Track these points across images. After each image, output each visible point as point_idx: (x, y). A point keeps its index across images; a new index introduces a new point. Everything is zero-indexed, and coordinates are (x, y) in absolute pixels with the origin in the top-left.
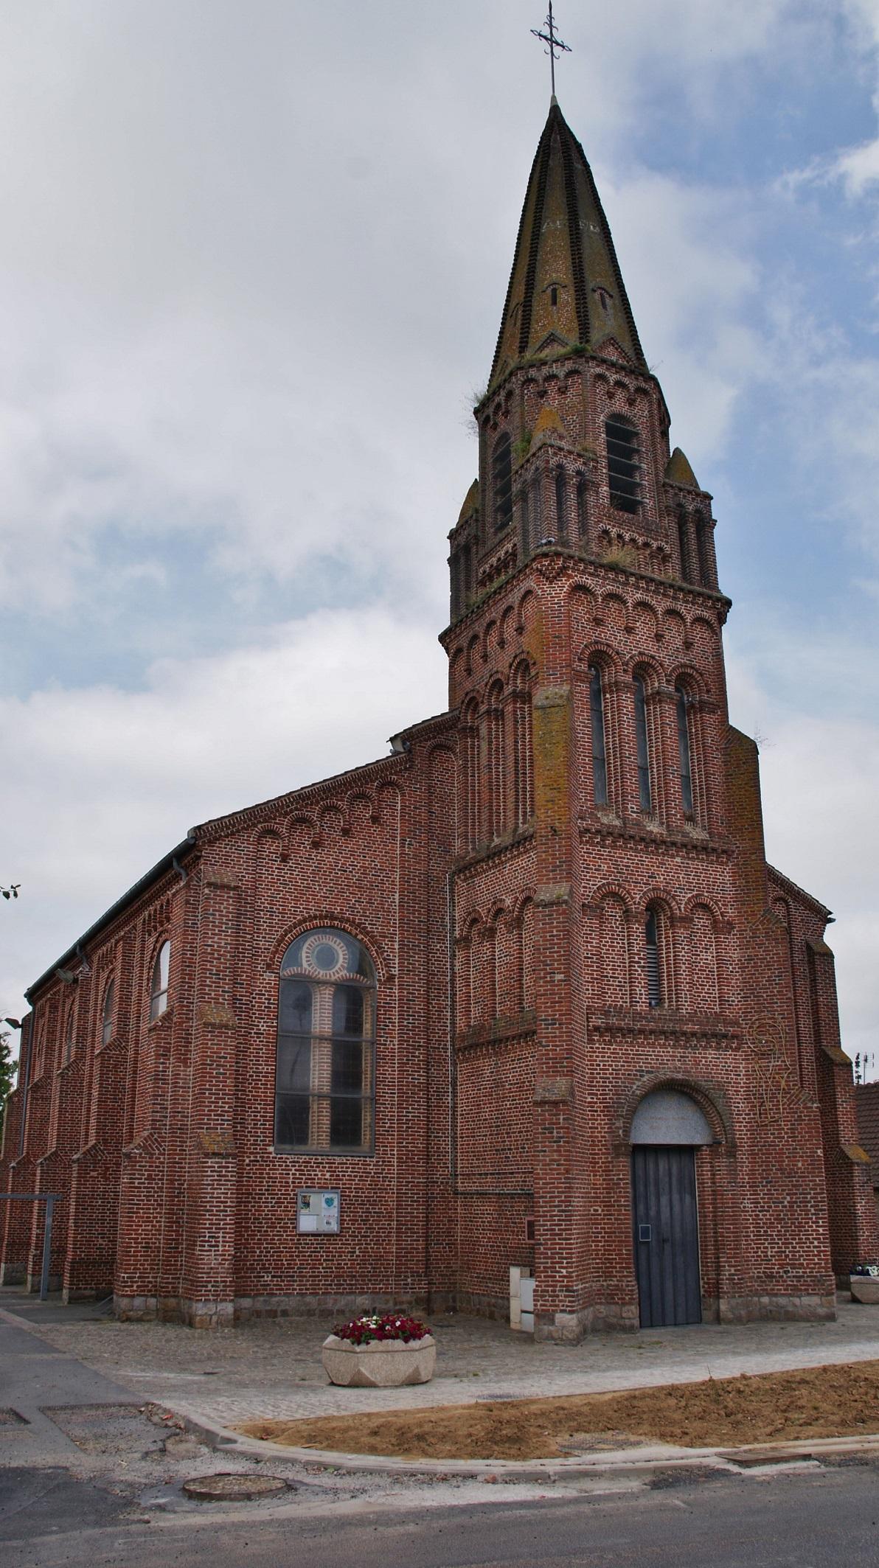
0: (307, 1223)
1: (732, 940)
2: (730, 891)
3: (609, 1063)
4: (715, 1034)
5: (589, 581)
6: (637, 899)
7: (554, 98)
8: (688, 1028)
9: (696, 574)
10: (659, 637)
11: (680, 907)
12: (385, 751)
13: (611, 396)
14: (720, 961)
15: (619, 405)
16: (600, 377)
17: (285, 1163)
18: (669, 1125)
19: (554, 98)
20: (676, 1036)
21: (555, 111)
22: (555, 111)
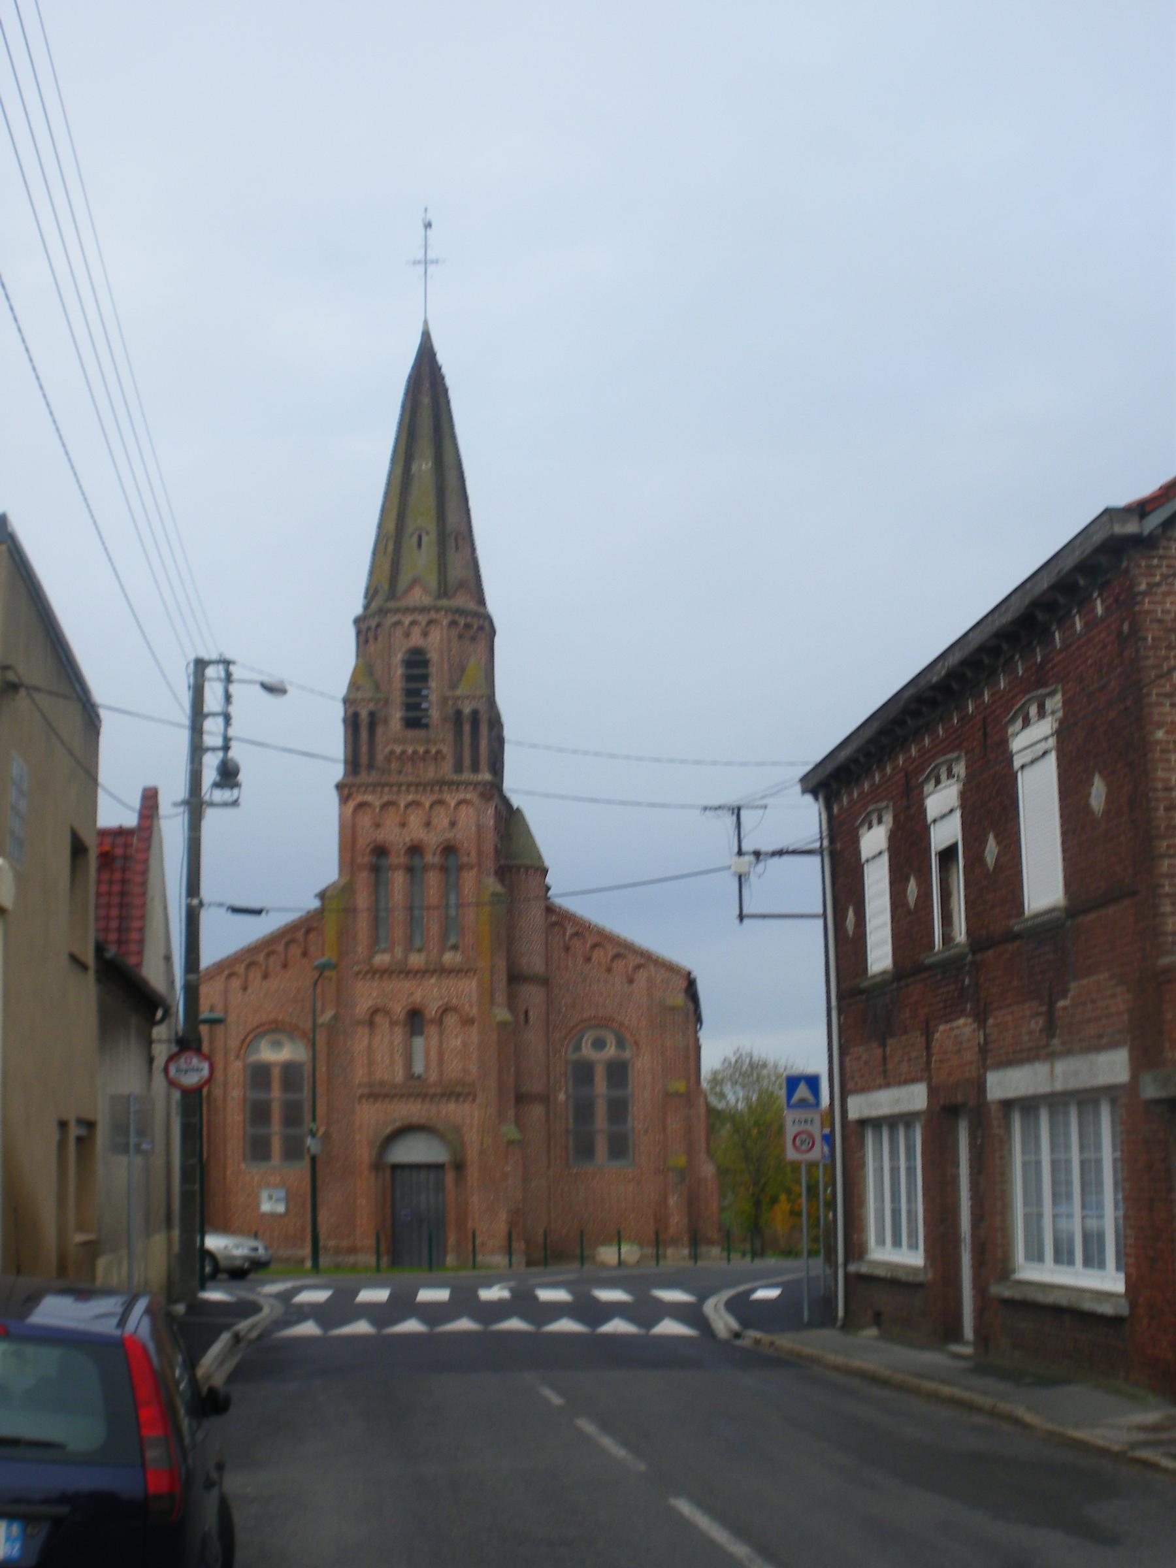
0: (266, 1207)
1: (474, 1030)
2: (474, 997)
3: (371, 1118)
4: (455, 1092)
5: (368, 798)
6: (399, 1010)
7: (426, 323)
8: (432, 1091)
9: (467, 762)
10: (428, 824)
11: (432, 1011)
12: (315, 904)
13: (407, 635)
14: (464, 1044)
15: (416, 640)
16: (398, 623)
17: (255, 1172)
18: (415, 1151)
19: (426, 323)
20: (424, 1096)
21: (426, 337)
22: (426, 337)
